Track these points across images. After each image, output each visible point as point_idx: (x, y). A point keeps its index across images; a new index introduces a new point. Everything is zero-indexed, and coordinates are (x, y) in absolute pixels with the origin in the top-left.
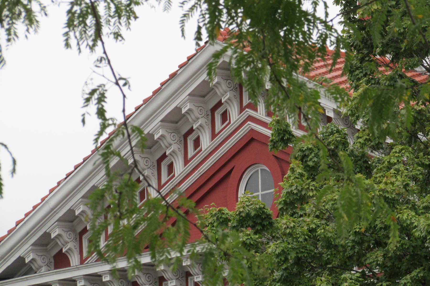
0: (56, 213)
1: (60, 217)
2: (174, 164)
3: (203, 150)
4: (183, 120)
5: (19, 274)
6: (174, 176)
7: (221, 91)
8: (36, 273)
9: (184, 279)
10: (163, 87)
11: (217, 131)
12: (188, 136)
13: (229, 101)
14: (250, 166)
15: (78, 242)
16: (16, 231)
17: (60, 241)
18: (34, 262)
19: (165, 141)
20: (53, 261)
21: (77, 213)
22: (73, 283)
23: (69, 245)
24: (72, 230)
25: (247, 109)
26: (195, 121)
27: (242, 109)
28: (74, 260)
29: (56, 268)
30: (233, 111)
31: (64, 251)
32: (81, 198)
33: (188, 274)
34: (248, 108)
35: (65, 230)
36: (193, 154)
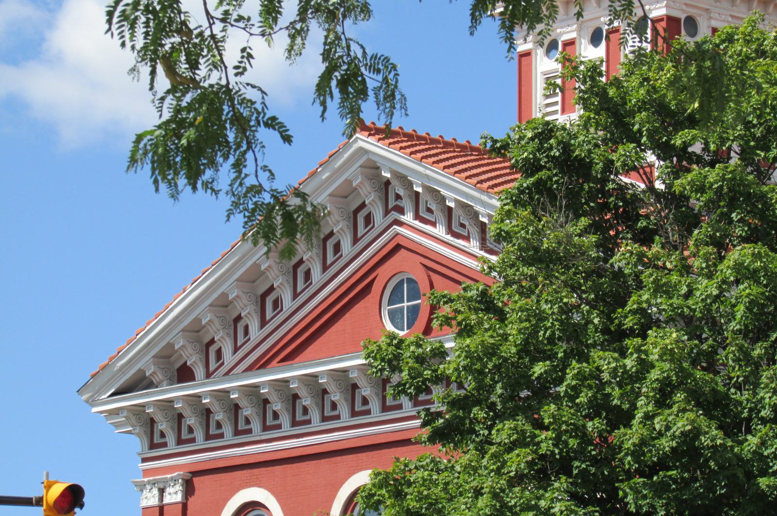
0: (181, 322)
1: (185, 327)
2: (312, 271)
3: (252, 339)
4: (261, 278)
5: (141, 386)
6: (311, 283)
7: (365, 191)
8: (157, 387)
9: (321, 397)
11: (359, 235)
12: (265, 299)
13: (281, 286)
14: (390, 279)
18: (184, 349)
20: (176, 374)
21: (204, 323)
22: (198, 399)
24: (198, 340)
25: (393, 212)
27: (387, 212)
28: (199, 372)
29: (179, 382)
30: (377, 211)
31: (188, 363)
32: (209, 306)
33: (325, 392)
36: (333, 259)
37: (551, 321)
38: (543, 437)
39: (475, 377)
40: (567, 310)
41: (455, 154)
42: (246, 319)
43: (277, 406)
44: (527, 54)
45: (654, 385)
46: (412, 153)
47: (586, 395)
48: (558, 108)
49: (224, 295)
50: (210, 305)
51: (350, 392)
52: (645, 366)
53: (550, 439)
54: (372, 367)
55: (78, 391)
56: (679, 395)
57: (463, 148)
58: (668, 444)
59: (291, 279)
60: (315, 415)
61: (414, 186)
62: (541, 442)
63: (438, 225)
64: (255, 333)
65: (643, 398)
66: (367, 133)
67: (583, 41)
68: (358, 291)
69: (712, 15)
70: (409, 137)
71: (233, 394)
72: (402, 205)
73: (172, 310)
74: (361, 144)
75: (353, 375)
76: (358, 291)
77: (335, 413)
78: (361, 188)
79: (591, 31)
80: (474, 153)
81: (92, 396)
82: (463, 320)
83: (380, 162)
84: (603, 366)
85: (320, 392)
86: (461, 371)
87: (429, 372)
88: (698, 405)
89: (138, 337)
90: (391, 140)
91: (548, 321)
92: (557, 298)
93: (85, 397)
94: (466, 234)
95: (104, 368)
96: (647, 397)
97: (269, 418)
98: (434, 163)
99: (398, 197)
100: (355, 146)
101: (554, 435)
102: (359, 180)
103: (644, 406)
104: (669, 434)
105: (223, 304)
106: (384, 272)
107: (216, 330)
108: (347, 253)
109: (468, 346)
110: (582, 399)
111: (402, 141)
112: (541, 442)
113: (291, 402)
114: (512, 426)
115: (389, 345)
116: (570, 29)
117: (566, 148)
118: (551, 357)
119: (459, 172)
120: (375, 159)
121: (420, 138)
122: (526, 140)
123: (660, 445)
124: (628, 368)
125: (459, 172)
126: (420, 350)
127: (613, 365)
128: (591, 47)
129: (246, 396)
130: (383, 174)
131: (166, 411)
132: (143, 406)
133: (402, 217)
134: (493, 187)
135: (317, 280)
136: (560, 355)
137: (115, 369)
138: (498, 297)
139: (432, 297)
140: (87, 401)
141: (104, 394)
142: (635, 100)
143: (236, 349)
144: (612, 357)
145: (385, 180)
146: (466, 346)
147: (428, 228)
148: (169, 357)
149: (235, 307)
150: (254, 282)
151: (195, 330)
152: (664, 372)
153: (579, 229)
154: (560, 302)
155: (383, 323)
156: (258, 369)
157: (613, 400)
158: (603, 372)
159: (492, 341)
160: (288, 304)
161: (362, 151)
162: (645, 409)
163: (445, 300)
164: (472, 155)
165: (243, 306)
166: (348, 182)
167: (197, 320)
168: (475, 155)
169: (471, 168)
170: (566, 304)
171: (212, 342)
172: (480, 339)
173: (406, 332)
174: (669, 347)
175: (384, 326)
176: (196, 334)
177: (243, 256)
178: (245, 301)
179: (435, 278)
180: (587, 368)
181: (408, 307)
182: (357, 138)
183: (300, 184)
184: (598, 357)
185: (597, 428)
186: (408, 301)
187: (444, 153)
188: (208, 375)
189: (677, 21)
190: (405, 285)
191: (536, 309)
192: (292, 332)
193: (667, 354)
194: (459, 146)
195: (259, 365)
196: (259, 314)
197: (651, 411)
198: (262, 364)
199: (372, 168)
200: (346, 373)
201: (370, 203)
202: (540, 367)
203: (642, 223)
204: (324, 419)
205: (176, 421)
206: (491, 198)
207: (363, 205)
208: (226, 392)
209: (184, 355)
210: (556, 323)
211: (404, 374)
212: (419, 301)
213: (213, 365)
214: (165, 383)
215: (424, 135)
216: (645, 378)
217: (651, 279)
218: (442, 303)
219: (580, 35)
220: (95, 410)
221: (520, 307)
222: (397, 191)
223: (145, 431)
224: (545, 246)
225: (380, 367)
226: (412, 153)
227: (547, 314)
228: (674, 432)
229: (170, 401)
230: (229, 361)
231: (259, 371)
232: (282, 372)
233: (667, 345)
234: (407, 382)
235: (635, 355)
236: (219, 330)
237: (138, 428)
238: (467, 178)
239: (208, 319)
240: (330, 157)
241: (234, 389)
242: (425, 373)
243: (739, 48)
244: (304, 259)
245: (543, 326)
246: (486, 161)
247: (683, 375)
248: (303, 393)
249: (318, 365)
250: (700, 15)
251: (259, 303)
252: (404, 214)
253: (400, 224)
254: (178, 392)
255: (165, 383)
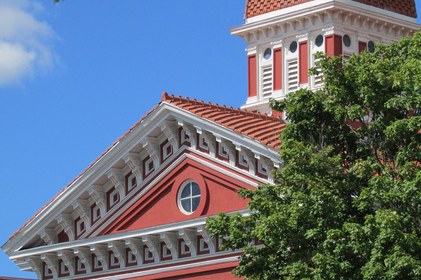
0: (61, 208)
3: (102, 217)
5: (36, 245)
6: (136, 186)
8: (47, 245)
9: (143, 249)
10: (149, 115)
11: (164, 158)
15: (74, 226)
16: (35, 219)
17: (113, 180)
18: (63, 223)
19: (95, 197)
21: (74, 208)
23: (68, 230)
24: (71, 218)
25: (184, 145)
26: (150, 152)
27: (180, 146)
28: (71, 236)
29: (59, 242)
30: (175, 145)
31: (65, 231)
34: (184, 144)
35: (98, 190)
37: (317, 205)
38: (315, 272)
39: (273, 238)
40: (325, 198)
41: (219, 112)
42: (98, 206)
43: (118, 255)
44: (253, 56)
45: (382, 242)
46: (196, 112)
47: (339, 248)
48: (272, 86)
49: (86, 192)
50: (78, 198)
51: (160, 247)
52: (375, 232)
53: (319, 273)
54: (212, 232)
55: (1, 247)
56: (396, 247)
57: (222, 109)
58: (393, 274)
59: (125, 185)
60: (139, 260)
61: (197, 130)
62: (314, 275)
63: (210, 152)
64: (104, 214)
65: (374, 249)
66: (170, 101)
67: (285, 49)
68: (164, 190)
69: (358, 34)
70: (193, 103)
71: (92, 249)
72: (189, 141)
73: (56, 201)
74: (166, 107)
75: (163, 237)
76: (164, 190)
77: (151, 259)
78: (165, 131)
79: (290, 43)
80: (228, 112)
81: (10, 250)
82: (265, 205)
83: (177, 117)
84: (351, 231)
85: (142, 247)
86: (265, 235)
87: (246, 235)
88: (408, 252)
89: (36, 216)
90: (184, 105)
91: (315, 205)
92: (320, 192)
93: (5, 250)
94: (227, 158)
95: (16, 234)
96: (377, 249)
97: (113, 262)
98: (209, 117)
99: (187, 137)
100: (163, 108)
101: (321, 271)
102: (165, 127)
103: (375, 254)
104: (393, 268)
105: (86, 197)
106: (179, 179)
107: (81, 213)
108: (157, 168)
109: (269, 221)
110: (337, 250)
111: (189, 105)
112: (314, 275)
113: (125, 252)
114: (297, 266)
115: (222, 219)
116: (278, 42)
117: (320, 106)
118: (315, 226)
119: (224, 122)
120: (174, 115)
121: (198, 103)
122: (296, 102)
123: (389, 275)
124: (365, 232)
125: (224, 122)
126: (240, 223)
127: (357, 230)
128: (290, 53)
129: (99, 249)
130: (179, 124)
131: (52, 258)
132: (39, 255)
133: (189, 148)
134: (243, 131)
135: (140, 184)
136: (320, 225)
137: (23, 235)
138: (279, 192)
139: (241, 193)
140: (7, 253)
141: (17, 249)
142: (360, 80)
143: (93, 223)
144: (356, 226)
145: (179, 127)
146: (268, 221)
147: (205, 154)
148: (54, 228)
149: (92, 199)
150: (103, 185)
151: (69, 213)
152: (387, 234)
153: (327, 153)
154: (322, 194)
155: (178, 208)
156: (105, 234)
157: (354, 250)
158: (351, 235)
159: (282, 217)
160: (123, 197)
161: (167, 111)
162: (377, 256)
163: (249, 194)
164: (227, 113)
165: (97, 199)
166: (159, 128)
167: (71, 207)
168: (229, 113)
169: (229, 120)
170: (325, 195)
171: (79, 219)
172: (276, 217)
173: (192, 213)
174: (392, 220)
175: (179, 210)
176: (69, 215)
177: (97, 171)
178: (98, 196)
179: (209, 182)
180: (339, 232)
181: (193, 199)
182: (164, 104)
183: (131, 130)
184: (348, 226)
185: (347, 267)
186: (193, 195)
187: (213, 112)
188: (76, 238)
189: (340, 37)
190: (191, 186)
191: (308, 198)
192: (126, 213)
193: (391, 224)
194: (219, 108)
195: (106, 232)
196: (106, 203)
197: (380, 257)
198: (107, 232)
199: (172, 121)
200: (158, 236)
201: (171, 140)
202: (311, 232)
203: (359, 149)
204: (145, 262)
205: (58, 263)
206: (243, 137)
207: (167, 141)
208: (88, 247)
209: (63, 227)
210: (320, 207)
211: (231, 236)
212: (200, 195)
213: (79, 232)
214: (51, 242)
215: (200, 102)
216: (377, 238)
217: (376, 182)
218: (246, 196)
219: (283, 46)
220: (11, 258)
221: (299, 197)
222: (186, 134)
223: (40, 270)
224: (312, 162)
225: (216, 232)
226: (196, 112)
227: (314, 201)
228: (397, 267)
229: (55, 253)
230: (88, 230)
231: (107, 235)
232: (121, 236)
233: (390, 219)
234: (233, 241)
235: (369, 225)
236: (83, 212)
237: (36, 268)
238: (229, 126)
239: (77, 206)
240: (148, 115)
241: (93, 246)
242: (243, 235)
243: (415, 50)
244: (132, 172)
245: (312, 208)
246: (235, 117)
247: (399, 236)
248: (133, 247)
249: (142, 232)
250: (352, 34)
251: (106, 197)
252: (190, 146)
253: (188, 152)
254: (60, 248)
255: (51, 242)
